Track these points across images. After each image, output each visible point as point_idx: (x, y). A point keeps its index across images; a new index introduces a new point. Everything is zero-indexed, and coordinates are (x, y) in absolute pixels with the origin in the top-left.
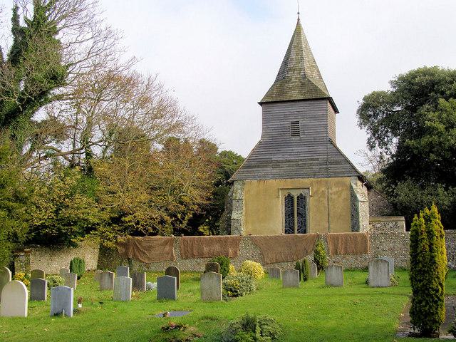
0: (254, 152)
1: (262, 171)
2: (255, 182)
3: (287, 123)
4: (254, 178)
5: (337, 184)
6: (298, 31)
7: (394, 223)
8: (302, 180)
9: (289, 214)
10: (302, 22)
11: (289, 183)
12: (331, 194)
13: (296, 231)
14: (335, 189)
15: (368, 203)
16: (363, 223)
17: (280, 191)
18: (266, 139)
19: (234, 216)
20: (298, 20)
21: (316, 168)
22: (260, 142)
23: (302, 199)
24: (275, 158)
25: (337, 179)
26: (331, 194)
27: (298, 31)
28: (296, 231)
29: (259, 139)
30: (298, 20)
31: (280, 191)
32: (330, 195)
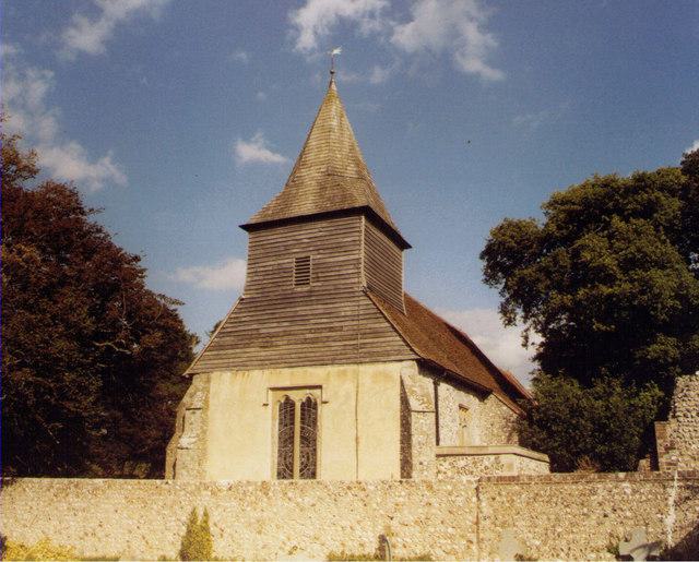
11: (286, 377)
16: (422, 458)
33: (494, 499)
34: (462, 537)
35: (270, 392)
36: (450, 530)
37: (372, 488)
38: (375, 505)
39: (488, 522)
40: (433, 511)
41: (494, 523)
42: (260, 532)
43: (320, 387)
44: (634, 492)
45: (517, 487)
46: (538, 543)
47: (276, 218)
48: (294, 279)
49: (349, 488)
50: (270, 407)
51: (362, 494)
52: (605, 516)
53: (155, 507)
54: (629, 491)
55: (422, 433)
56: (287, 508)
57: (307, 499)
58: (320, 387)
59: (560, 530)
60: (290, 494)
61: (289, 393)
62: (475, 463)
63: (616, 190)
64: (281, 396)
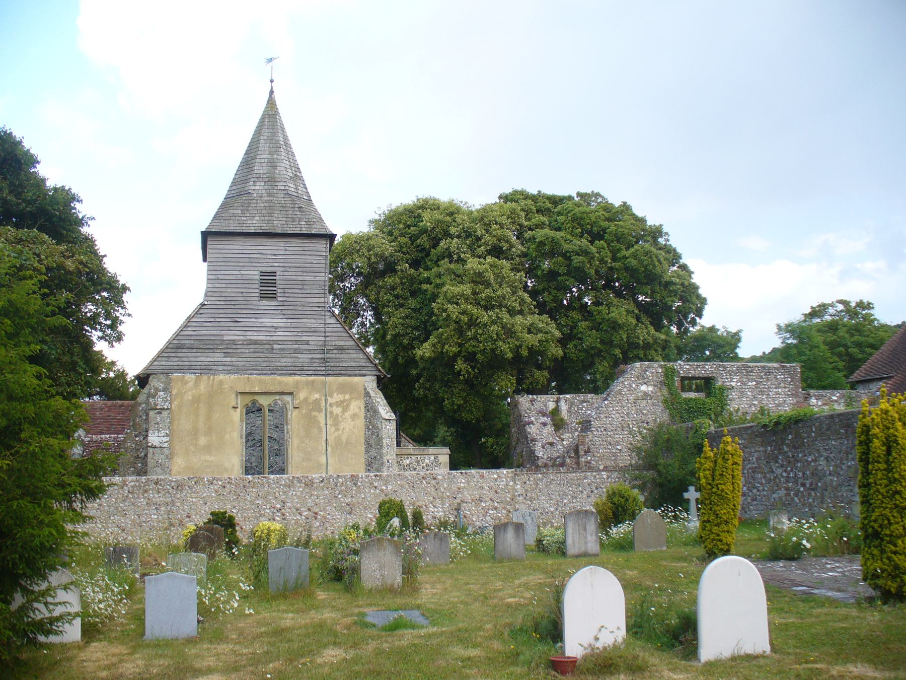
0: (774, 629)
1: (204, 359)
2: (190, 377)
3: (254, 274)
4: (190, 369)
5: (342, 389)
6: (271, 103)
7: (432, 458)
8: (278, 378)
9: (253, 440)
10: (277, 97)
11: (257, 383)
12: (331, 405)
13: (267, 470)
14: (337, 397)
15: (394, 423)
16: (388, 457)
17: (239, 396)
18: (632, 622)
19: (154, 439)
20: (272, 92)
21: (304, 358)
22: (203, 305)
23: (279, 413)
24: (229, 336)
25: (341, 379)
26: (331, 405)
27: (271, 103)
28: (267, 470)
29: (200, 299)
30: (272, 92)
31: (239, 396)
32: (329, 409)
33: (525, 483)
34: (504, 508)
35: (239, 396)
36: (496, 504)
37: (440, 477)
38: (442, 490)
39: (521, 498)
40: (485, 492)
41: (525, 498)
42: (350, 514)
43: (291, 394)
44: (608, 477)
45: (540, 475)
46: (552, 509)
47: (273, 231)
48: (279, 291)
49: (423, 478)
50: (239, 410)
51: (433, 482)
52: (592, 492)
53: (249, 498)
54: (605, 477)
55: (389, 437)
56: (374, 494)
57: (390, 487)
58: (291, 394)
59: (565, 501)
60: (376, 484)
61: (257, 397)
62: (418, 462)
63: (875, 664)
64: (248, 399)
